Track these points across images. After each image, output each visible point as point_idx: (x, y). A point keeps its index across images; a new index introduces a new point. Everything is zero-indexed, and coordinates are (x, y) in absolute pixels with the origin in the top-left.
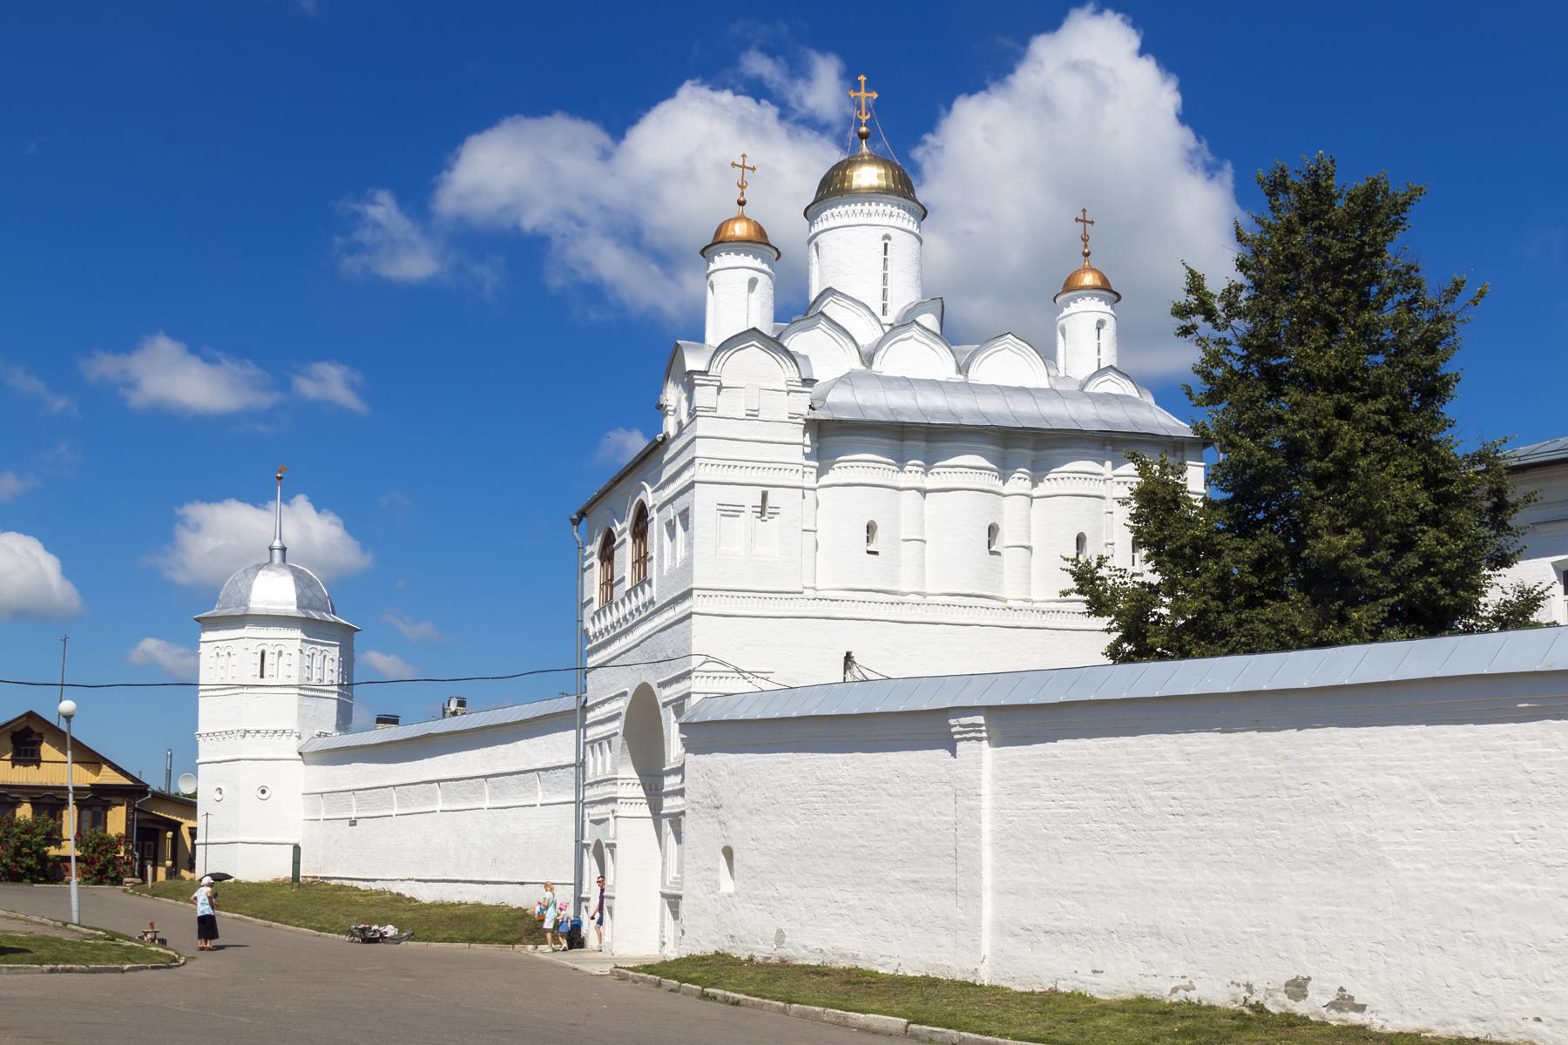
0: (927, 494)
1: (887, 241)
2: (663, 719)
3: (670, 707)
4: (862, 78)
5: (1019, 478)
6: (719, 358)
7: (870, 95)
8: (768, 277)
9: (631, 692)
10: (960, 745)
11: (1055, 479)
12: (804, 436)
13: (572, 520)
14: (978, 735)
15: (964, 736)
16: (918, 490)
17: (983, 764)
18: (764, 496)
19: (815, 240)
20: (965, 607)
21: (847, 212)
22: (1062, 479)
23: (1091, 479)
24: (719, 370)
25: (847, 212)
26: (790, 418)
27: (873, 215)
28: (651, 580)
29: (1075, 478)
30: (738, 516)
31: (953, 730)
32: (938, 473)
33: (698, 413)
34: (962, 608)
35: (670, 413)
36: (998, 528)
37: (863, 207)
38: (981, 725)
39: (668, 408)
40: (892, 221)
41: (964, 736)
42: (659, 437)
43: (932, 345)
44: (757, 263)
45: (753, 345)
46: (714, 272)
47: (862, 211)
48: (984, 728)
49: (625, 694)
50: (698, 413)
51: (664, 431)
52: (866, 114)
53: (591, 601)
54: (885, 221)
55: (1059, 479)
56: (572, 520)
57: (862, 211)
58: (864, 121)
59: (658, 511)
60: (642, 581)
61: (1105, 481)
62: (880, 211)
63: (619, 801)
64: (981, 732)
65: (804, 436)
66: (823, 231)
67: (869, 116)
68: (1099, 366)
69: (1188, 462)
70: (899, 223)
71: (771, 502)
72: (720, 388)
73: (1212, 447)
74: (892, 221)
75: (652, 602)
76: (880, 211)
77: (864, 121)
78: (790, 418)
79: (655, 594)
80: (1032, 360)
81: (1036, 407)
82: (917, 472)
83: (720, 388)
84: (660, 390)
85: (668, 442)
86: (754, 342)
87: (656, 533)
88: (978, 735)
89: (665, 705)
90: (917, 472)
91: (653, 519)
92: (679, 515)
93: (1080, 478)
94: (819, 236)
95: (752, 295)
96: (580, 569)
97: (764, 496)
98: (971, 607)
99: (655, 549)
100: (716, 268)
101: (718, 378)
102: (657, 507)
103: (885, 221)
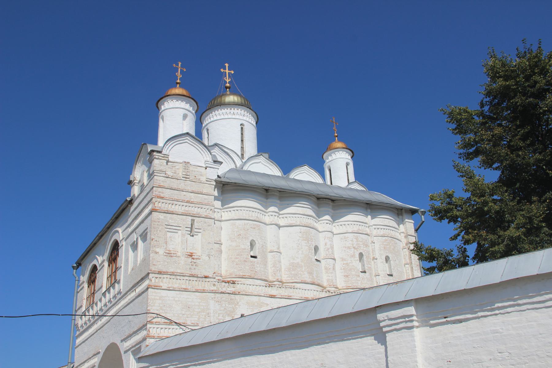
0: (281, 228)
1: (242, 126)
2: (124, 362)
3: (130, 352)
4: (227, 65)
5: (327, 223)
6: (167, 147)
7: (230, 72)
8: (193, 115)
9: (102, 351)
10: (389, 337)
11: (344, 225)
12: (214, 191)
13: (73, 267)
14: (409, 324)
15: (393, 327)
16: (276, 225)
17: (417, 349)
18: (193, 221)
19: (206, 127)
20: (305, 290)
21: (223, 113)
22: (348, 225)
23: (362, 226)
24: (168, 152)
25: (223, 113)
26: (207, 181)
27: (236, 115)
28: (119, 280)
29: (354, 225)
30: (177, 233)
31: (382, 324)
32: (286, 217)
33: (155, 174)
34: (304, 290)
35: (136, 184)
36: (318, 249)
37: (231, 111)
38: (412, 316)
39: (135, 181)
40: (245, 118)
41: (393, 327)
42: (129, 199)
43: (270, 167)
44: (187, 106)
45: (186, 142)
46: (164, 110)
47: (230, 113)
48: (415, 318)
49: (99, 353)
50: (155, 174)
51: (132, 195)
52: (229, 79)
53: (81, 307)
54: (241, 117)
56: (73, 267)
57: (230, 113)
58: (228, 82)
59: (125, 240)
60: (113, 279)
61: (369, 227)
62: (239, 113)
63: (186, 201)
64: (412, 321)
65: (214, 191)
66: (211, 122)
67: (230, 80)
69: (406, 220)
70: (248, 119)
71: (196, 225)
72: (168, 162)
73: (417, 214)
74: (245, 118)
75: (120, 292)
76: (239, 113)
77: (228, 82)
78: (207, 181)
79: (122, 288)
80: (317, 179)
81: (331, 190)
82: (275, 216)
83: (168, 162)
84: (130, 171)
85: (134, 200)
86: (187, 138)
87: (124, 254)
88: (409, 324)
89: (126, 352)
90: (275, 216)
91: (122, 245)
92: (140, 236)
93: (357, 225)
94: (209, 125)
95: (185, 122)
96: (76, 291)
97: (193, 221)
98: (308, 290)
99: (123, 263)
100: (165, 108)
101: (166, 156)
102: (125, 239)
103: (241, 117)
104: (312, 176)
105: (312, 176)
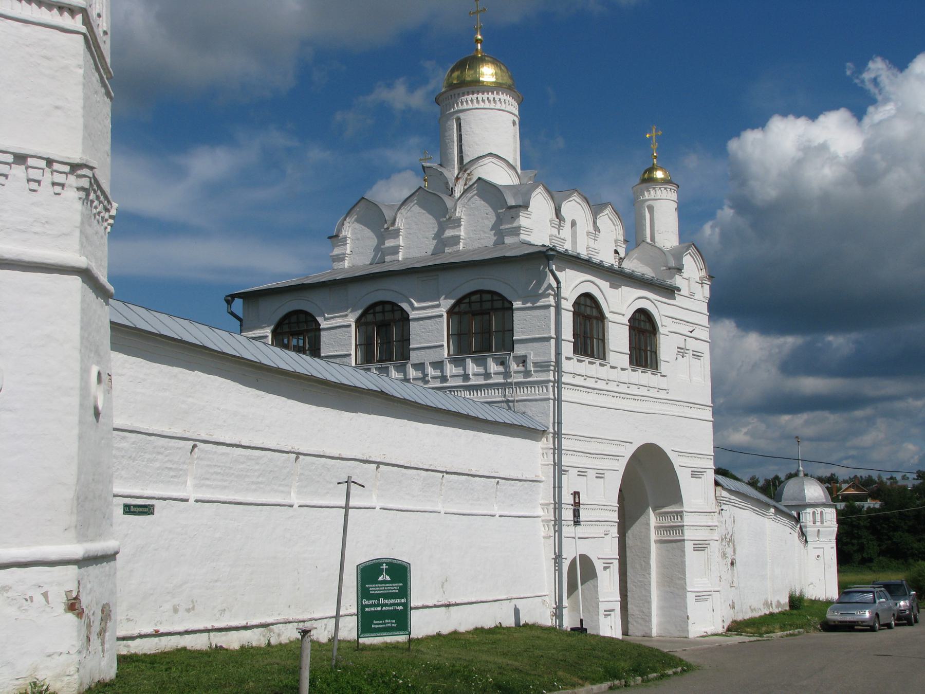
21: (500, 99)
55: (591, 474)
68: (563, 309)
104: (698, 264)
105: (698, 264)
